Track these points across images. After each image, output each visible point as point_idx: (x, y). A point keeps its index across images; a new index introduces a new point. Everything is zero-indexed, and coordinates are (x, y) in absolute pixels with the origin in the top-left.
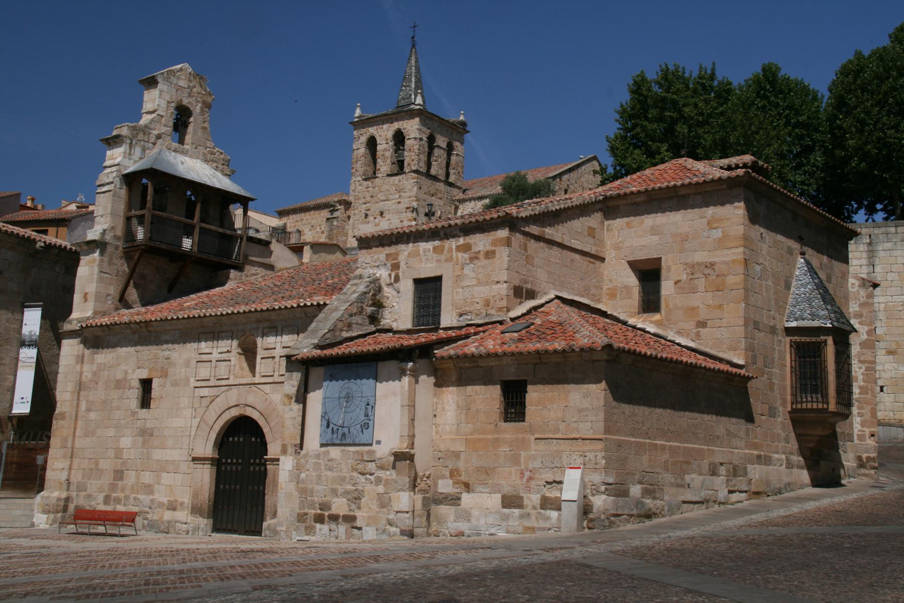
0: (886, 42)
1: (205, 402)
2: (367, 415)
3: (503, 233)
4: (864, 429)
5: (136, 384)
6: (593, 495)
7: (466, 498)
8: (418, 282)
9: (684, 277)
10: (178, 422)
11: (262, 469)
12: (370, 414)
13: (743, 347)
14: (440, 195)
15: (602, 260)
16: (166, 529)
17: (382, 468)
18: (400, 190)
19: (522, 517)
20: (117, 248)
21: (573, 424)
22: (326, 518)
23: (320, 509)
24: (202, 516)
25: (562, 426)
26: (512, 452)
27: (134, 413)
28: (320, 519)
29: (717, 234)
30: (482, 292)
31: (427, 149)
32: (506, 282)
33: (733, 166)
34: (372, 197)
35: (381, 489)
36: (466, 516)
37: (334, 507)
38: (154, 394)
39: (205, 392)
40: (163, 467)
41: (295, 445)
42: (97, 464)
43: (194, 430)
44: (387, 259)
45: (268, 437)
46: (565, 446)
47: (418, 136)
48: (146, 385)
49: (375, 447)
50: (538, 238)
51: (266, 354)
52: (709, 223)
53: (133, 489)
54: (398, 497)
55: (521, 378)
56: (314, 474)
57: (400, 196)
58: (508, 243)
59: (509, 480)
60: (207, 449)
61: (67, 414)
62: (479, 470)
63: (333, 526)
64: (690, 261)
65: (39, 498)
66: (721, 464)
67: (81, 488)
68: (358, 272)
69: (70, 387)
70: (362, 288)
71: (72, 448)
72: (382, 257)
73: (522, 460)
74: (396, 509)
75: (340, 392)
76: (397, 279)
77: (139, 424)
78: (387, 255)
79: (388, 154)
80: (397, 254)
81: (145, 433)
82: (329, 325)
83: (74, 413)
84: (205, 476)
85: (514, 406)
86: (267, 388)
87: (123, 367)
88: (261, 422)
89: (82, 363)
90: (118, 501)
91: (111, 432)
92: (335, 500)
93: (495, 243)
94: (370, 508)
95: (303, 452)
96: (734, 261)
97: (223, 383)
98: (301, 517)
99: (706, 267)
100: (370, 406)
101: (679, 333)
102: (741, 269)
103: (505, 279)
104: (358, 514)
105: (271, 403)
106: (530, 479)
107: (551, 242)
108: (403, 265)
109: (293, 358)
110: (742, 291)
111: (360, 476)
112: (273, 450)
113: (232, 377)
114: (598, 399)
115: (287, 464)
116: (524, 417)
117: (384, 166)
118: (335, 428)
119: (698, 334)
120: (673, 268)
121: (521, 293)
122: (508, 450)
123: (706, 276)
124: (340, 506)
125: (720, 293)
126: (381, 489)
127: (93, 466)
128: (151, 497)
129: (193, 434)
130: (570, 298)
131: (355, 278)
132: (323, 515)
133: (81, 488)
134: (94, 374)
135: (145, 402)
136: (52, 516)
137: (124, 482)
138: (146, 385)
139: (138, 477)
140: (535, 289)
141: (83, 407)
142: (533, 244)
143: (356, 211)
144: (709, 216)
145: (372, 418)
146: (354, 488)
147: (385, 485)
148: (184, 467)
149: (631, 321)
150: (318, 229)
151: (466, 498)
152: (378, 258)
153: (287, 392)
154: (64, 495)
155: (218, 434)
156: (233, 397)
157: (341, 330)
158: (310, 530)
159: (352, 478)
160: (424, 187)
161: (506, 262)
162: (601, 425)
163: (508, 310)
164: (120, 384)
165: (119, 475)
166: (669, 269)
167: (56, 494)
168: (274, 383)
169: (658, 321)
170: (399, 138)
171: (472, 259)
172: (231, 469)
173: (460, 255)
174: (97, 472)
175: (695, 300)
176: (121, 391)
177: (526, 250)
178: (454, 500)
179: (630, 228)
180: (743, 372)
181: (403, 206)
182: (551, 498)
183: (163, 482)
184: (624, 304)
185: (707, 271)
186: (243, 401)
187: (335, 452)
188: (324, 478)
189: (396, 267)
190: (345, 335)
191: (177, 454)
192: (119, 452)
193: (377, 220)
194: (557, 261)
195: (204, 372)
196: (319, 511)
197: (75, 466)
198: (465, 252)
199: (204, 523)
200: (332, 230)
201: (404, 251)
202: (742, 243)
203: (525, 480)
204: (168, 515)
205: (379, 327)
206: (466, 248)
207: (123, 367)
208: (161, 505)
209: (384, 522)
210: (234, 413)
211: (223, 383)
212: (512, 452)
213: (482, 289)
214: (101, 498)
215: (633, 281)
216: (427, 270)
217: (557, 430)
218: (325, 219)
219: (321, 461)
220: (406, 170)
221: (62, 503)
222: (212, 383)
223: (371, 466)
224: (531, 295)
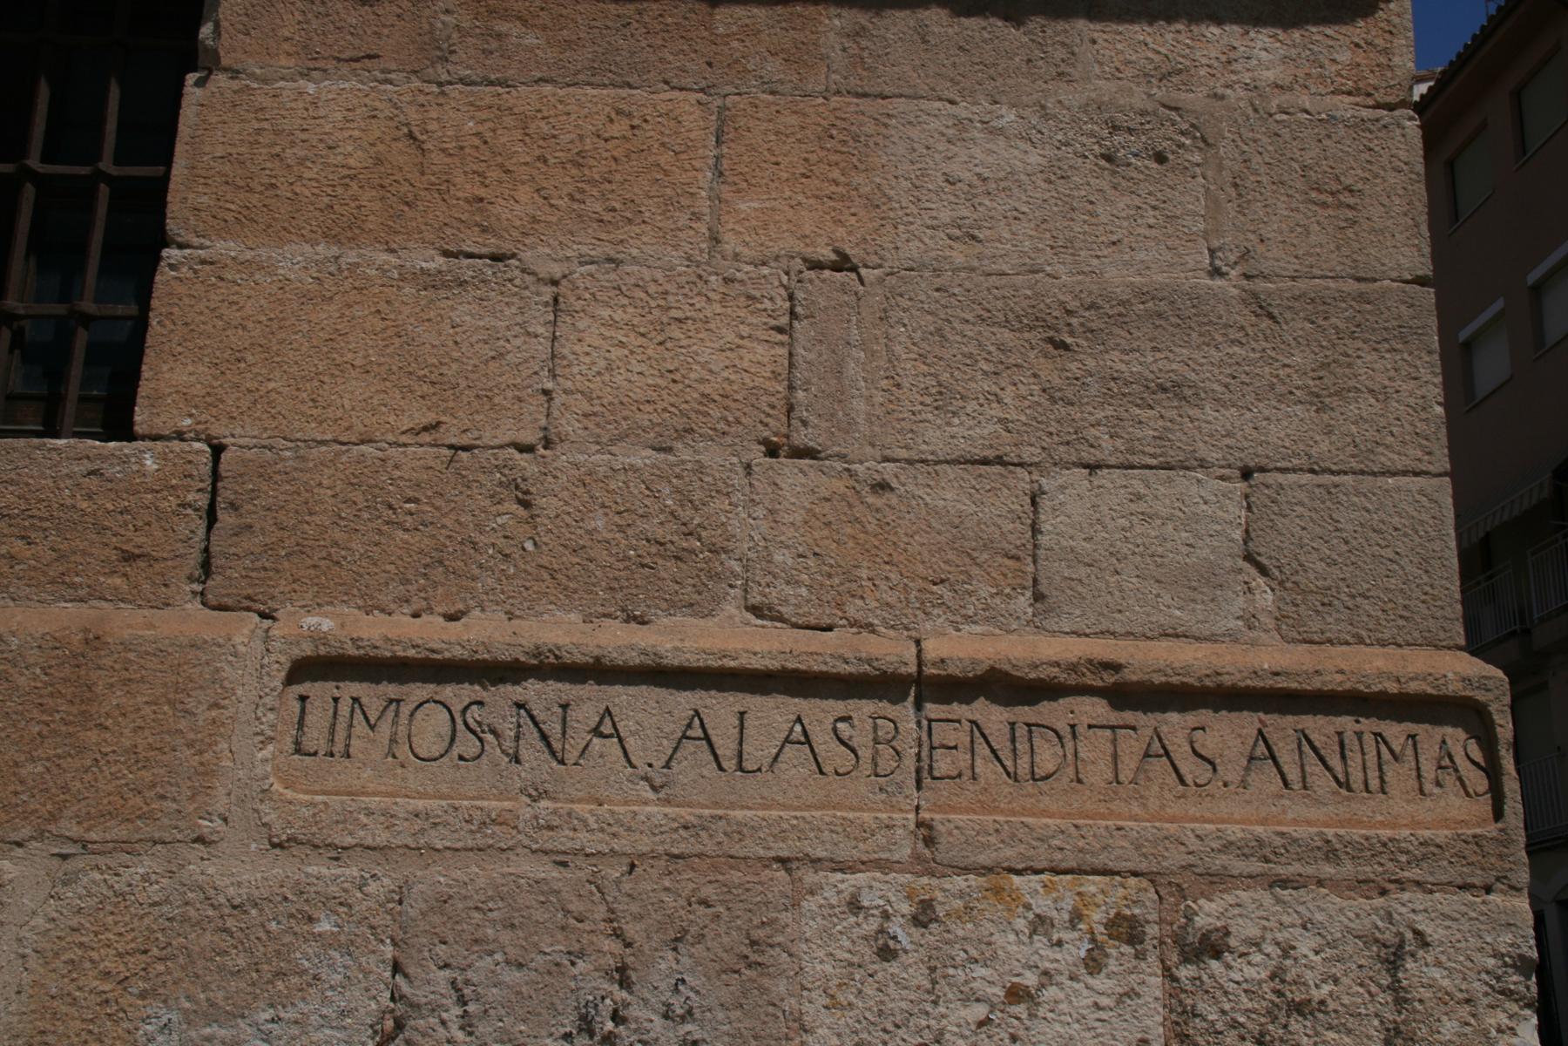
15: (274, 619)
46: (810, 787)
55: (180, 148)
114: (1335, 196)
217: (688, 560)
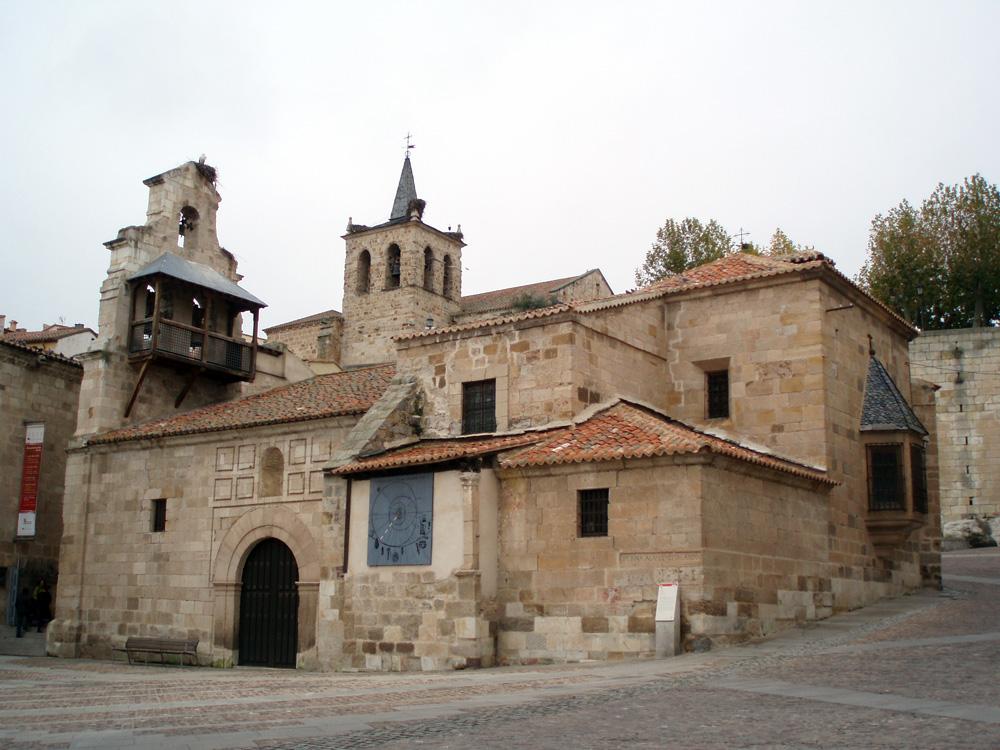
3: (565, 329)
4: (929, 538)
5: (148, 505)
6: (691, 614)
7: (539, 621)
9: (757, 378)
10: (197, 546)
11: (293, 594)
12: (427, 530)
13: (824, 452)
14: (438, 311)
17: (443, 590)
18: (396, 306)
20: (122, 359)
21: (665, 537)
22: (377, 648)
23: (371, 638)
24: (226, 646)
26: (593, 570)
27: (146, 537)
28: (370, 649)
29: (792, 329)
30: (543, 395)
31: (424, 264)
32: (570, 384)
33: (798, 260)
34: (365, 313)
35: (442, 614)
36: (541, 641)
37: (386, 634)
38: (170, 514)
39: (226, 512)
40: (181, 594)
41: (337, 568)
42: (109, 590)
43: (214, 553)
44: (430, 362)
45: (300, 561)
47: (414, 249)
48: (160, 505)
50: (603, 335)
51: (293, 469)
52: (782, 319)
53: (149, 619)
54: (464, 623)
56: (361, 599)
57: (396, 313)
58: (571, 339)
59: (591, 600)
60: (229, 572)
61: (75, 538)
63: (387, 656)
64: (763, 360)
66: (809, 577)
68: (397, 377)
69: (77, 508)
70: (402, 395)
71: (82, 574)
72: (425, 359)
73: (606, 578)
74: (461, 636)
75: (390, 508)
78: (430, 357)
79: (383, 269)
80: (442, 357)
82: (370, 434)
83: (82, 537)
84: (227, 606)
86: (297, 508)
87: (134, 487)
88: (291, 545)
89: (89, 482)
92: (386, 628)
93: (556, 340)
94: (429, 636)
95: (346, 576)
96: (811, 360)
97: (246, 502)
99: (781, 366)
101: (752, 439)
102: (819, 367)
103: (569, 380)
104: (415, 642)
105: (301, 523)
106: (616, 598)
107: (613, 341)
108: (448, 368)
109: (334, 471)
110: (821, 392)
111: (416, 600)
112: (306, 574)
113: (255, 496)
115: (328, 589)
116: (606, 531)
117: (378, 280)
118: (386, 548)
119: (774, 440)
120: (744, 368)
121: (587, 396)
122: (588, 567)
123: (782, 376)
124: (392, 634)
125: (797, 394)
126: (442, 614)
127: (105, 594)
128: (170, 627)
129: (213, 558)
130: (635, 402)
131: (394, 383)
132: (374, 644)
133: (94, 616)
134: (103, 494)
135: (159, 524)
137: (139, 611)
139: (154, 605)
140: (598, 391)
141: (92, 531)
142: (596, 343)
143: (350, 329)
144: (782, 311)
145: (429, 535)
146: (410, 614)
147: (446, 610)
148: (205, 595)
149: (698, 427)
150: (309, 349)
151: (539, 621)
152: (421, 361)
153: (327, 510)
154: (76, 624)
155: (242, 559)
156: (257, 517)
157: (383, 441)
160: (422, 302)
161: (570, 361)
162: (697, 537)
163: (573, 415)
164: (131, 506)
165: (133, 603)
166: (739, 369)
167: (67, 623)
168: (304, 501)
169: (728, 427)
172: (290, 595)
173: (515, 354)
174: (110, 600)
176: (131, 513)
177: (589, 348)
179: (694, 326)
180: (825, 477)
181: (399, 322)
182: (641, 620)
183: (181, 610)
185: (782, 371)
186: (269, 522)
188: (373, 604)
189: (441, 370)
190: (387, 446)
191: (194, 581)
192: (132, 579)
193: (371, 338)
194: (621, 362)
195: (224, 490)
196: (369, 641)
197: (86, 594)
198: (521, 351)
200: (324, 349)
202: (820, 339)
203: (609, 600)
205: (422, 438)
206: (523, 347)
207: (134, 487)
209: (446, 651)
210: (260, 535)
211: (246, 502)
212: (593, 570)
215: (699, 382)
216: (477, 374)
218: (316, 338)
219: (370, 585)
220: (402, 283)
221: (74, 632)
222: (233, 502)
223: (429, 589)
224: (596, 398)
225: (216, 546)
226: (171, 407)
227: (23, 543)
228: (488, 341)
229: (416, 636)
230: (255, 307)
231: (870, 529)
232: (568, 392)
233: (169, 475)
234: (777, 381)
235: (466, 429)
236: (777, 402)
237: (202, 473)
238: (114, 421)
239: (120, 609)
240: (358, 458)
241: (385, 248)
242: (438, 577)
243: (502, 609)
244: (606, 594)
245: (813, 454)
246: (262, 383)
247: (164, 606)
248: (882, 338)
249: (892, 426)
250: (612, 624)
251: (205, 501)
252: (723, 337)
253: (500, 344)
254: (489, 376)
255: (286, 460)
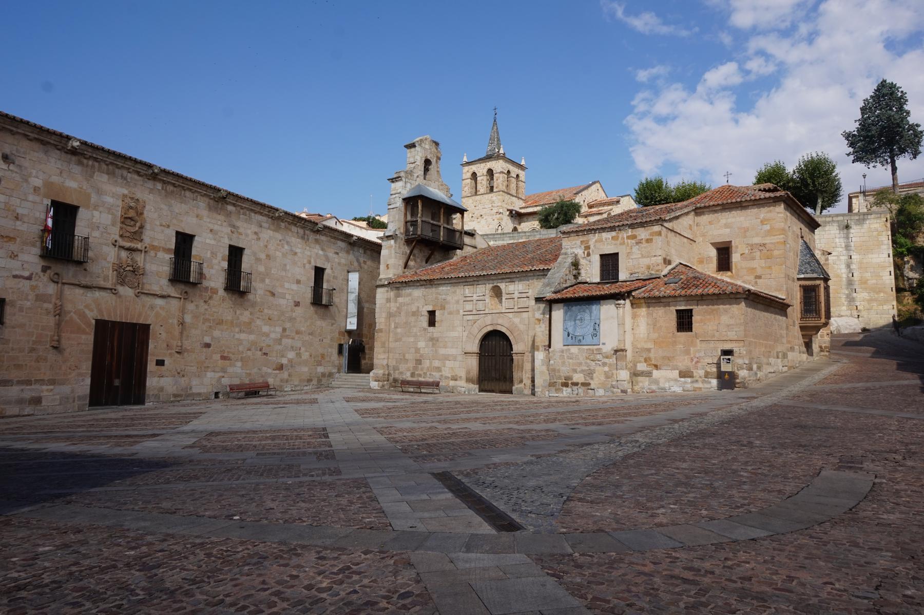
0: (911, 120)
1: (470, 323)
2: (595, 329)
3: (657, 228)
7: (656, 373)
8: (603, 257)
10: (455, 334)
16: (452, 391)
17: (607, 357)
19: (692, 382)
24: (473, 383)
25: (717, 334)
27: (425, 329)
29: (768, 227)
35: (606, 369)
39: (470, 317)
40: (446, 358)
48: (432, 314)
49: (601, 346)
51: (508, 296)
59: (684, 362)
60: (475, 347)
62: (664, 358)
65: (371, 374)
67: (396, 368)
69: (384, 315)
72: (578, 242)
76: (589, 255)
77: (429, 335)
80: (588, 241)
81: (433, 340)
84: (473, 363)
85: (684, 322)
86: (511, 315)
88: (508, 333)
90: (420, 375)
91: (412, 339)
98: (552, 385)
100: (596, 325)
104: (591, 382)
108: (592, 247)
119: (756, 283)
124: (578, 378)
133: (396, 368)
134: (398, 308)
135: (432, 323)
136: (381, 383)
138: (432, 314)
148: (460, 358)
156: (489, 320)
158: (557, 390)
159: (586, 363)
165: (419, 362)
166: (737, 247)
170: (490, 172)
171: (637, 243)
175: (754, 264)
178: (649, 374)
184: (710, 268)
187: (574, 350)
189: (588, 248)
190: (565, 286)
192: (417, 350)
195: (469, 307)
199: (476, 387)
201: (593, 239)
204: (452, 383)
206: (634, 237)
208: (447, 378)
213: (645, 260)
214: (408, 374)
215: (713, 253)
223: (599, 357)
224: (669, 263)
225: (465, 334)
226: (424, 263)
227: (350, 332)
228: (614, 234)
229: (592, 379)
230: (462, 211)
231: (801, 327)
232: (660, 260)
233: (437, 298)
234: (758, 253)
235: (602, 279)
236: (758, 264)
237: (456, 298)
238: (400, 270)
239: (411, 365)
240: (555, 292)
241: (485, 171)
242: (604, 351)
243: (635, 366)
244: (692, 360)
245: (779, 290)
246: (468, 251)
247: (437, 363)
248: (805, 230)
249: (815, 275)
250: (695, 374)
251: (458, 311)
252: (728, 230)
253: (620, 236)
254: (616, 251)
255: (503, 291)
